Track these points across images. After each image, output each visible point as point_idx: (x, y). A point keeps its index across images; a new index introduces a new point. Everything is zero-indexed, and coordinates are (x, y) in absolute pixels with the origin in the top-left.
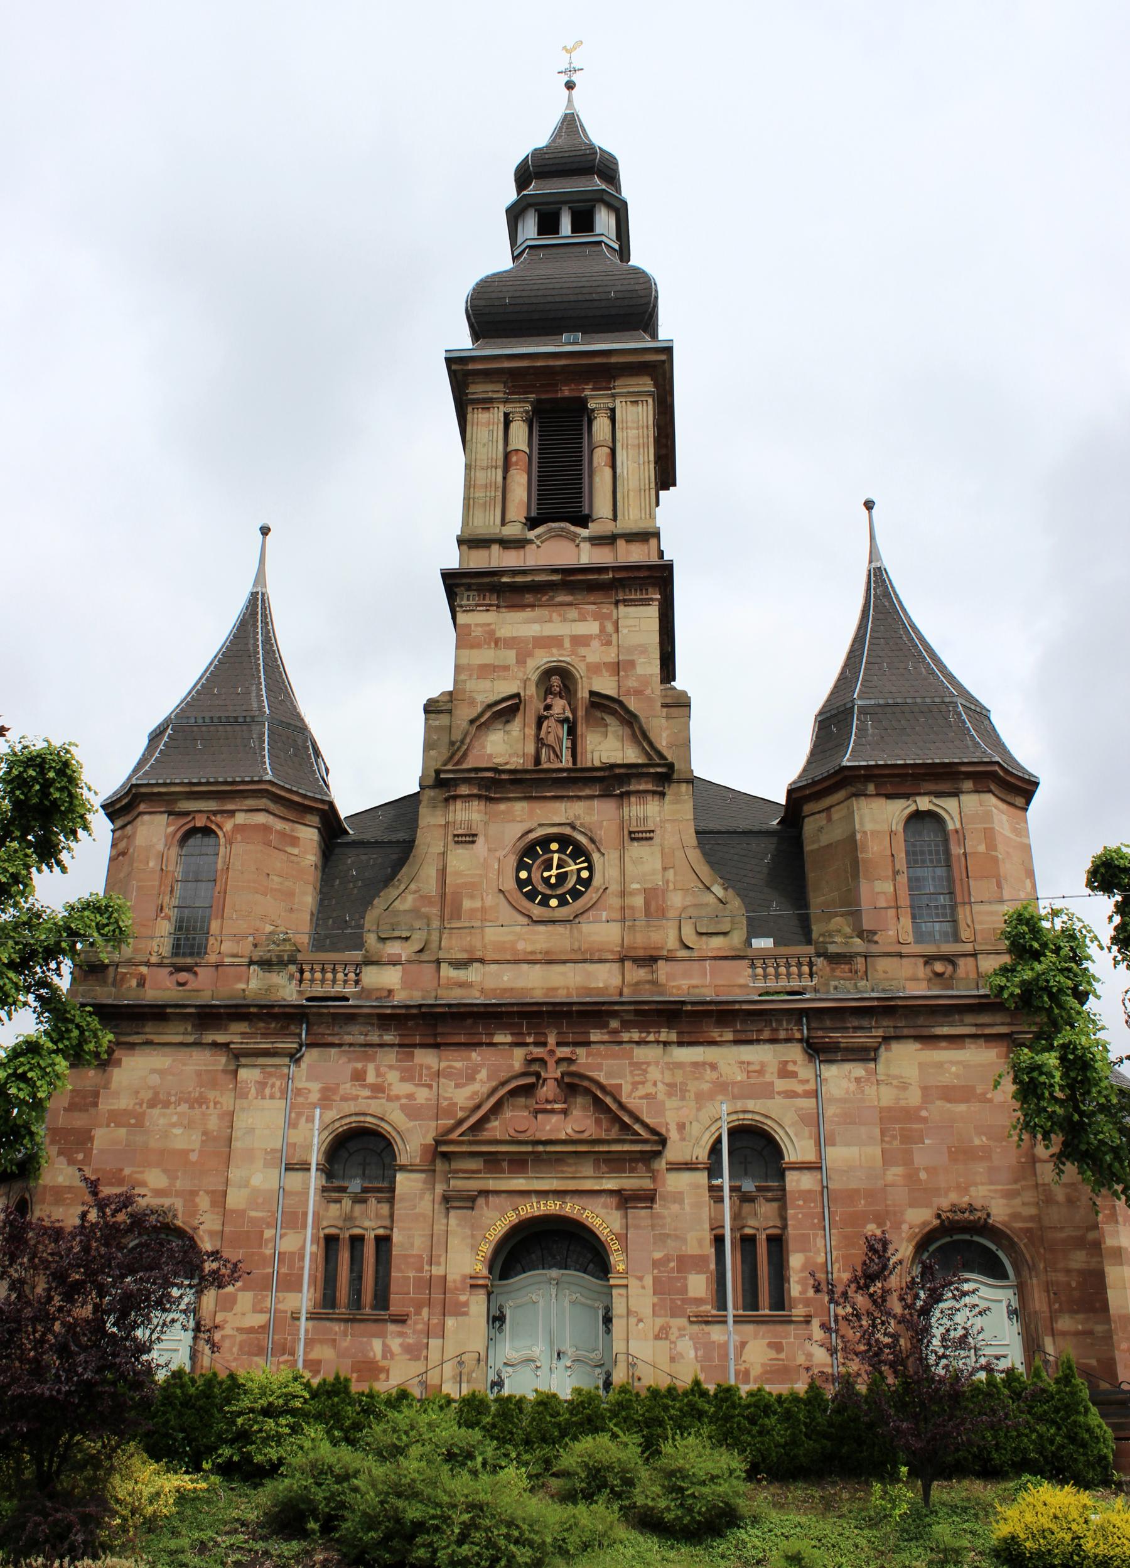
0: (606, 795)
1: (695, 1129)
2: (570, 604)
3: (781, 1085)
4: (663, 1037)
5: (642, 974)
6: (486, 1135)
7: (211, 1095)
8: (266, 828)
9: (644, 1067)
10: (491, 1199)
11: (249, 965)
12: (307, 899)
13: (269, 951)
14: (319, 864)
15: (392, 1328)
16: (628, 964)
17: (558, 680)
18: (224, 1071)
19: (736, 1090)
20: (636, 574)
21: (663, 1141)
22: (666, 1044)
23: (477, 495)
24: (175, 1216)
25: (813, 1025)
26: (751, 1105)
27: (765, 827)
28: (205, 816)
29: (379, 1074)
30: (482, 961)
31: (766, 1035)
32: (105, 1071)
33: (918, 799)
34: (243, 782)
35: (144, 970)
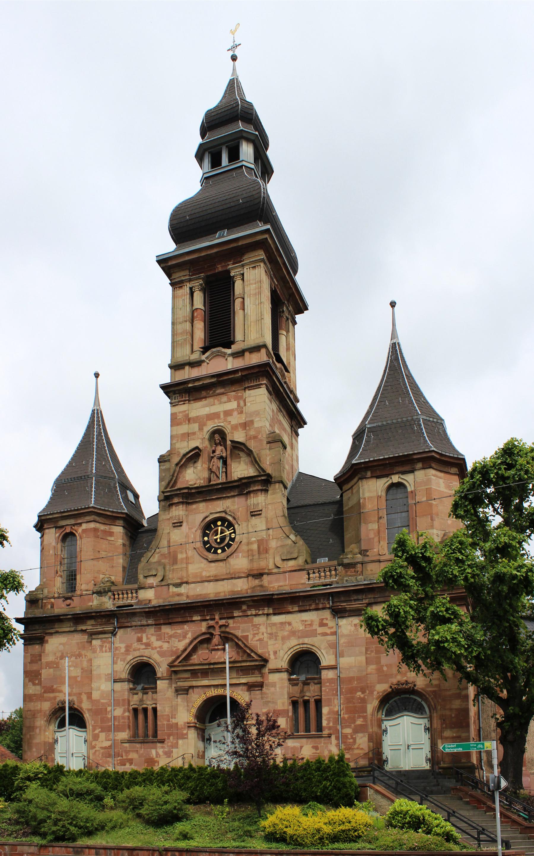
0: (240, 494)
1: (282, 653)
2: (223, 394)
3: (320, 630)
4: (266, 612)
5: (257, 582)
6: (191, 662)
7: (83, 652)
8: (96, 530)
9: (258, 626)
10: (195, 690)
11: (93, 594)
12: (120, 561)
13: (100, 587)
14: (127, 543)
15: (159, 745)
16: (250, 578)
17: (218, 436)
18: (87, 642)
19: (299, 634)
20: (252, 371)
21: (266, 661)
22: (268, 615)
23: (178, 339)
24: (74, 704)
25: (335, 600)
26: (306, 640)
27: (333, 500)
28: (70, 527)
29: (148, 639)
30: (187, 583)
31: (313, 606)
32: (42, 645)
33: (393, 477)
34: (82, 509)
35: (53, 600)
